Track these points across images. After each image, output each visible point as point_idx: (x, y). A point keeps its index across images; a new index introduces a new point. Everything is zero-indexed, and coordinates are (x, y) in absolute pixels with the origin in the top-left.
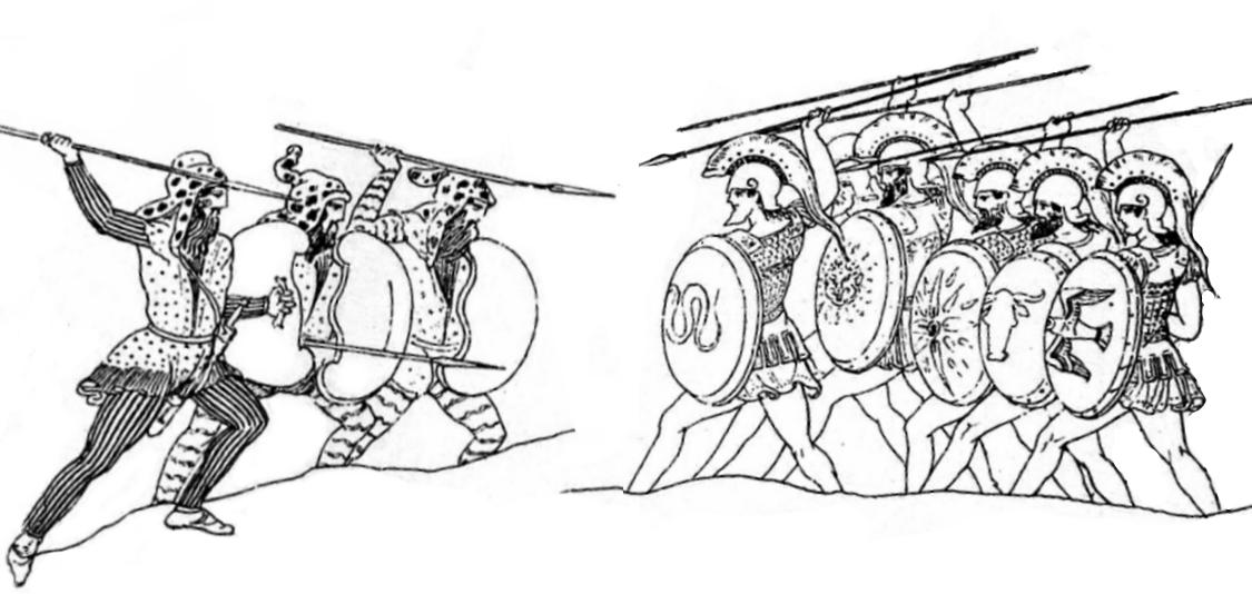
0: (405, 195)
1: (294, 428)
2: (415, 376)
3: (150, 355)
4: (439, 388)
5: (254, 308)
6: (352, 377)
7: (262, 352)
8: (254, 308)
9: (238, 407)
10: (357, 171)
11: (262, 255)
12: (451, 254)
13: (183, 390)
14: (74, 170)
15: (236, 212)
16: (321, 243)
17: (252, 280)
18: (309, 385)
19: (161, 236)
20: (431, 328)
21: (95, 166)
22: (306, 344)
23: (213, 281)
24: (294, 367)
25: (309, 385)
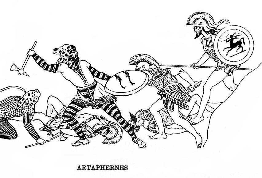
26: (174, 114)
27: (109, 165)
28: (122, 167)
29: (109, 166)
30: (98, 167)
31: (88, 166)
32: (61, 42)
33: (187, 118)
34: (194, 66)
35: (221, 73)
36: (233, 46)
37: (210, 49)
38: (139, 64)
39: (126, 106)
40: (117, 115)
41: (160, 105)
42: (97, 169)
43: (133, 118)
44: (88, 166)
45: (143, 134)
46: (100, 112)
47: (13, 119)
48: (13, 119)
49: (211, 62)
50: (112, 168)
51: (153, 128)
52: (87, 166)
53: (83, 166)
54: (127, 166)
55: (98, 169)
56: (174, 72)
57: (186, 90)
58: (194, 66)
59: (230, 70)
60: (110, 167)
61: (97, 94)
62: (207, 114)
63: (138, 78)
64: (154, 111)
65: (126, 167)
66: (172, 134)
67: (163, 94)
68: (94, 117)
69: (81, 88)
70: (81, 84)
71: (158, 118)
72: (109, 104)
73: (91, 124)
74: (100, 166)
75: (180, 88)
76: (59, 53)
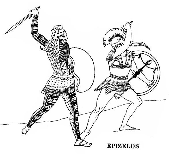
27: (126, 144)
28: (124, 145)
29: (110, 144)
30: (113, 145)
31: (129, 147)
32: (139, 59)
38: (113, 74)
42: (112, 148)
44: (129, 147)
47: (132, 128)
48: (132, 128)
50: (124, 147)
52: (130, 148)
53: (108, 144)
54: (138, 145)
55: (113, 147)
57: (113, 63)
60: (112, 145)
65: (137, 145)
66: (85, 131)
69: (76, 138)
74: (116, 145)
76: (146, 63)
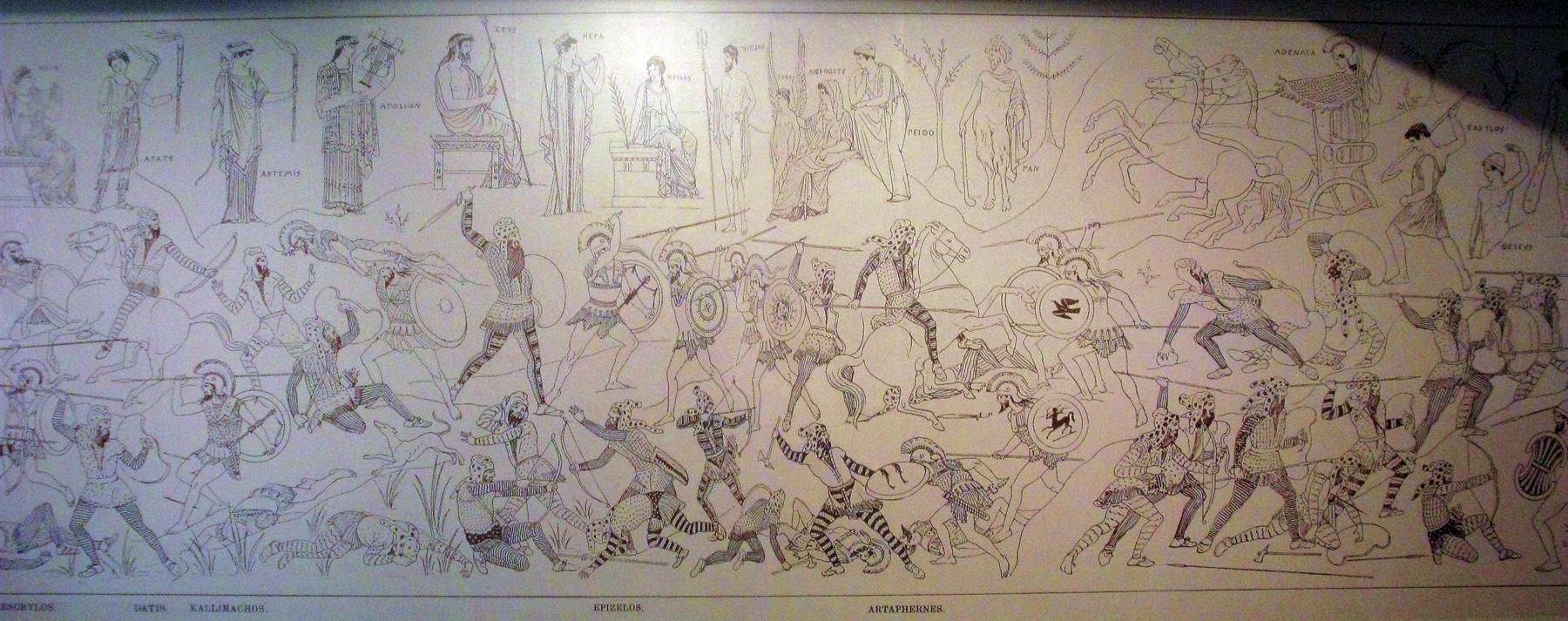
0: (1528, 289)
1: (1503, 388)
2: (1544, 358)
3: (1445, 372)
4: (1554, 362)
5: (1479, 345)
6: (1518, 365)
7: (1486, 361)
8: (1479, 345)
9: (1479, 384)
10: (1507, 283)
11: (1478, 323)
12: (1549, 308)
13: (1460, 383)
14: (1402, 305)
15: (1466, 309)
16: (1500, 314)
17: (1476, 336)
18: (1505, 371)
19: (1440, 324)
20: (1546, 338)
21: (1411, 303)
22: (1501, 354)
23: (1463, 339)
24: (1500, 363)
25: (1505, 371)
26: (967, 528)
33: (987, 533)
34: (997, 456)
35: (1039, 466)
36: (1056, 424)
37: (1021, 429)
39: (897, 516)
40: (884, 529)
41: (947, 513)
43: (906, 533)
45: (920, 557)
46: (859, 524)
49: (1024, 450)
51: (935, 545)
56: (967, 464)
58: (997, 456)
59: (1051, 461)
61: (856, 498)
62: (1016, 528)
63: (914, 473)
64: (936, 523)
67: (950, 498)
68: (852, 532)
70: (835, 483)
71: (943, 534)
72: (872, 512)
73: (848, 542)
75: (977, 489)
